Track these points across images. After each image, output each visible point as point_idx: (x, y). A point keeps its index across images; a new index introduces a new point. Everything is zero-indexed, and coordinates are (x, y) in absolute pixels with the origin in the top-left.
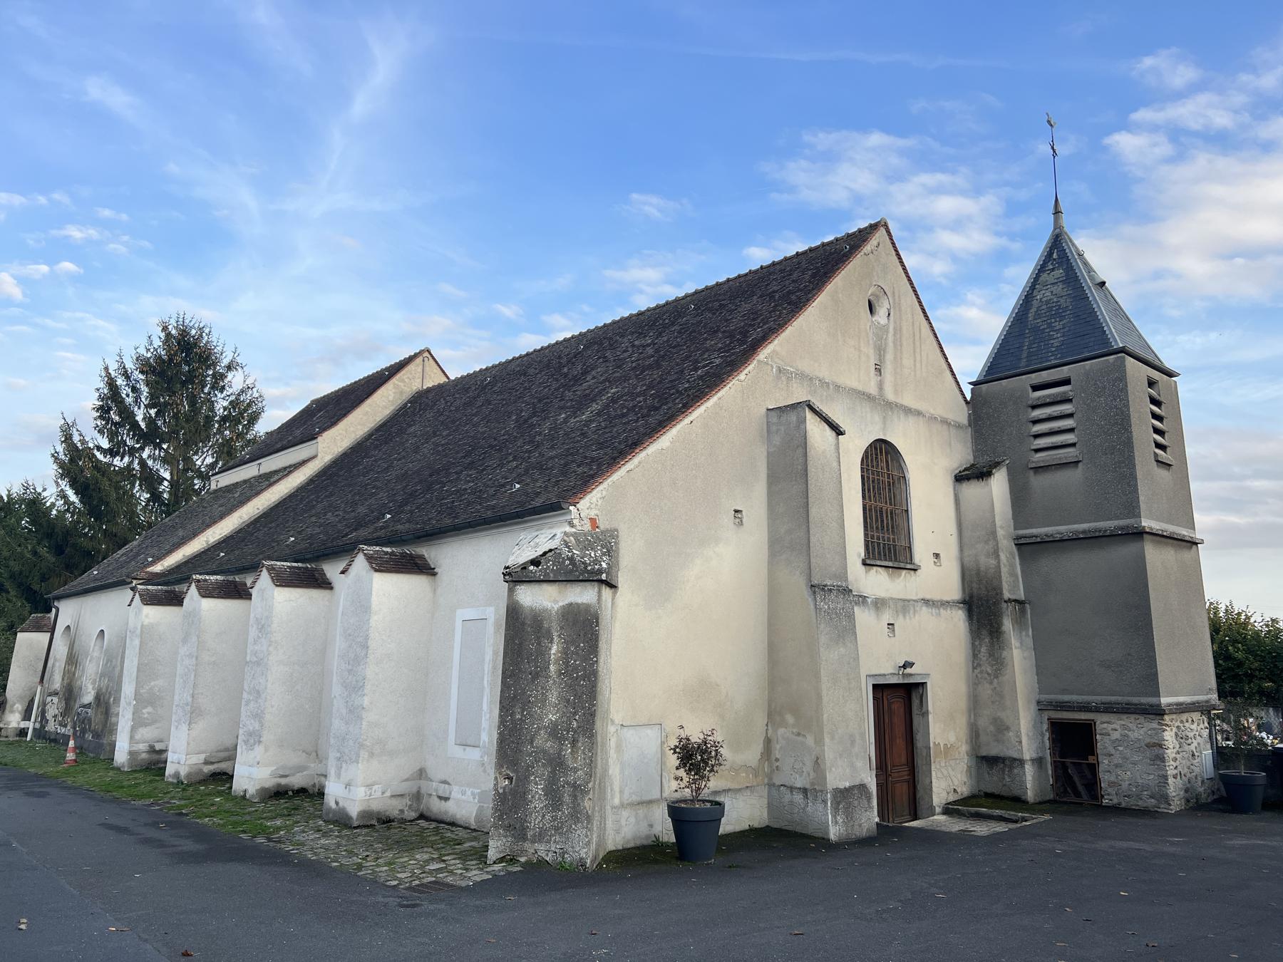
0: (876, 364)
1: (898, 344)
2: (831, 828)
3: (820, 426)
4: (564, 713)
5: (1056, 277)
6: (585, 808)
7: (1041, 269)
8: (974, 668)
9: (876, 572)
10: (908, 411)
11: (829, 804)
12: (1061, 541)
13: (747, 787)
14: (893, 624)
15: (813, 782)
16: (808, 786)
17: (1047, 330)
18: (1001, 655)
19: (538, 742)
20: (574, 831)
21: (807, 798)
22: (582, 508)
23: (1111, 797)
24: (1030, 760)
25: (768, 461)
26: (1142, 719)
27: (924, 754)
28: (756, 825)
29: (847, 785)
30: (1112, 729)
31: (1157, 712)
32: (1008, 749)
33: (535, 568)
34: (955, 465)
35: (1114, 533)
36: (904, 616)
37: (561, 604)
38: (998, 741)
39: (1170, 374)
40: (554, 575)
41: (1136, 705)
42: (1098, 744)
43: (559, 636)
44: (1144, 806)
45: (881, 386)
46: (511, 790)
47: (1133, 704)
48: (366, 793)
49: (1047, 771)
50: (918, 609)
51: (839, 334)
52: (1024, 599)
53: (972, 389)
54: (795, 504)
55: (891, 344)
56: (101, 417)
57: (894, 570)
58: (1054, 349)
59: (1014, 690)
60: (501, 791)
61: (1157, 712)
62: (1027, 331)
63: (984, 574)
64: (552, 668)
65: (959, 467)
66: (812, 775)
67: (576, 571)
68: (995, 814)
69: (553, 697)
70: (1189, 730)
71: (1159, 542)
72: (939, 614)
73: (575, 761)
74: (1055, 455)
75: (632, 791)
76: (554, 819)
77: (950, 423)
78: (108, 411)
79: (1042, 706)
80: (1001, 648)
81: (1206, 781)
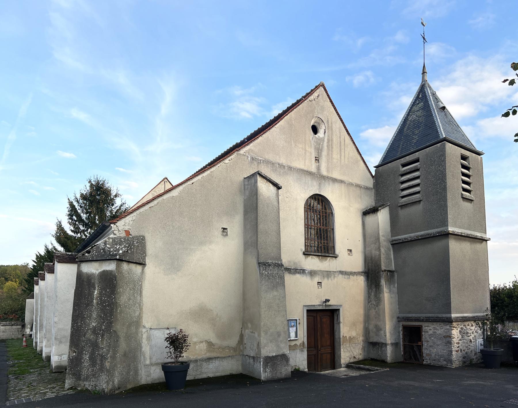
0: (316, 157)
1: (330, 147)
2: (262, 374)
3: (267, 184)
4: (99, 322)
5: (419, 107)
6: (106, 366)
7: (414, 104)
8: (369, 302)
9: (312, 258)
10: (335, 180)
11: (262, 363)
12: (411, 241)
13: (229, 356)
14: (321, 283)
15: (257, 354)
16: (255, 356)
17: (411, 135)
18: (379, 296)
19: (88, 336)
20: (101, 376)
21: (254, 361)
22: (119, 225)
23: (427, 361)
24: (390, 344)
25: (244, 204)
26: (442, 324)
27: (338, 341)
28: (234, 373)
29: (274, 354)
30: (429, 330)
31: (449, 321)
32: (381, 339)
33: (88, 254)
34: (364, 207)
35: (435, 235)
36: (328, 279)
37: (100, 271)
38: (377, 335)
39: (479, 154)
40: (96, 258)
41: (440, 318)
42: (423, 336)
43: (98, 286)
44: (441, 365)
45: (318, 168)
46: (75, 357)
47: (439, 318)
48: (58, 358)
49: (401, 349)
50: (336, 275)
51: (292, 142)
52: (394, 270)
53: (375, 170)
54: (253, 223)
55: (325, 147)
56: (70, 219)
57: (322, 257)
58: (413, 144)
59: (384, 312)
60: (71, 358)
61: (449, 321)
62: (403, 137)
63: (374, 259)
64: (95, 301)
65: (366, 208)
66: (257, 350)
67: (105, 255)
68: (366, 368)
69: (94, 315)
70: (469, 330)
71: (460, 239)
72: (349, 278)
73: (104, 344)
74: (411, 198)
75: (157, 358)
76: (93, 371)
77: (361, 187)
78: (72, 216)
79: (400, 319)
80: (380, 293)
81: (477, 353)
